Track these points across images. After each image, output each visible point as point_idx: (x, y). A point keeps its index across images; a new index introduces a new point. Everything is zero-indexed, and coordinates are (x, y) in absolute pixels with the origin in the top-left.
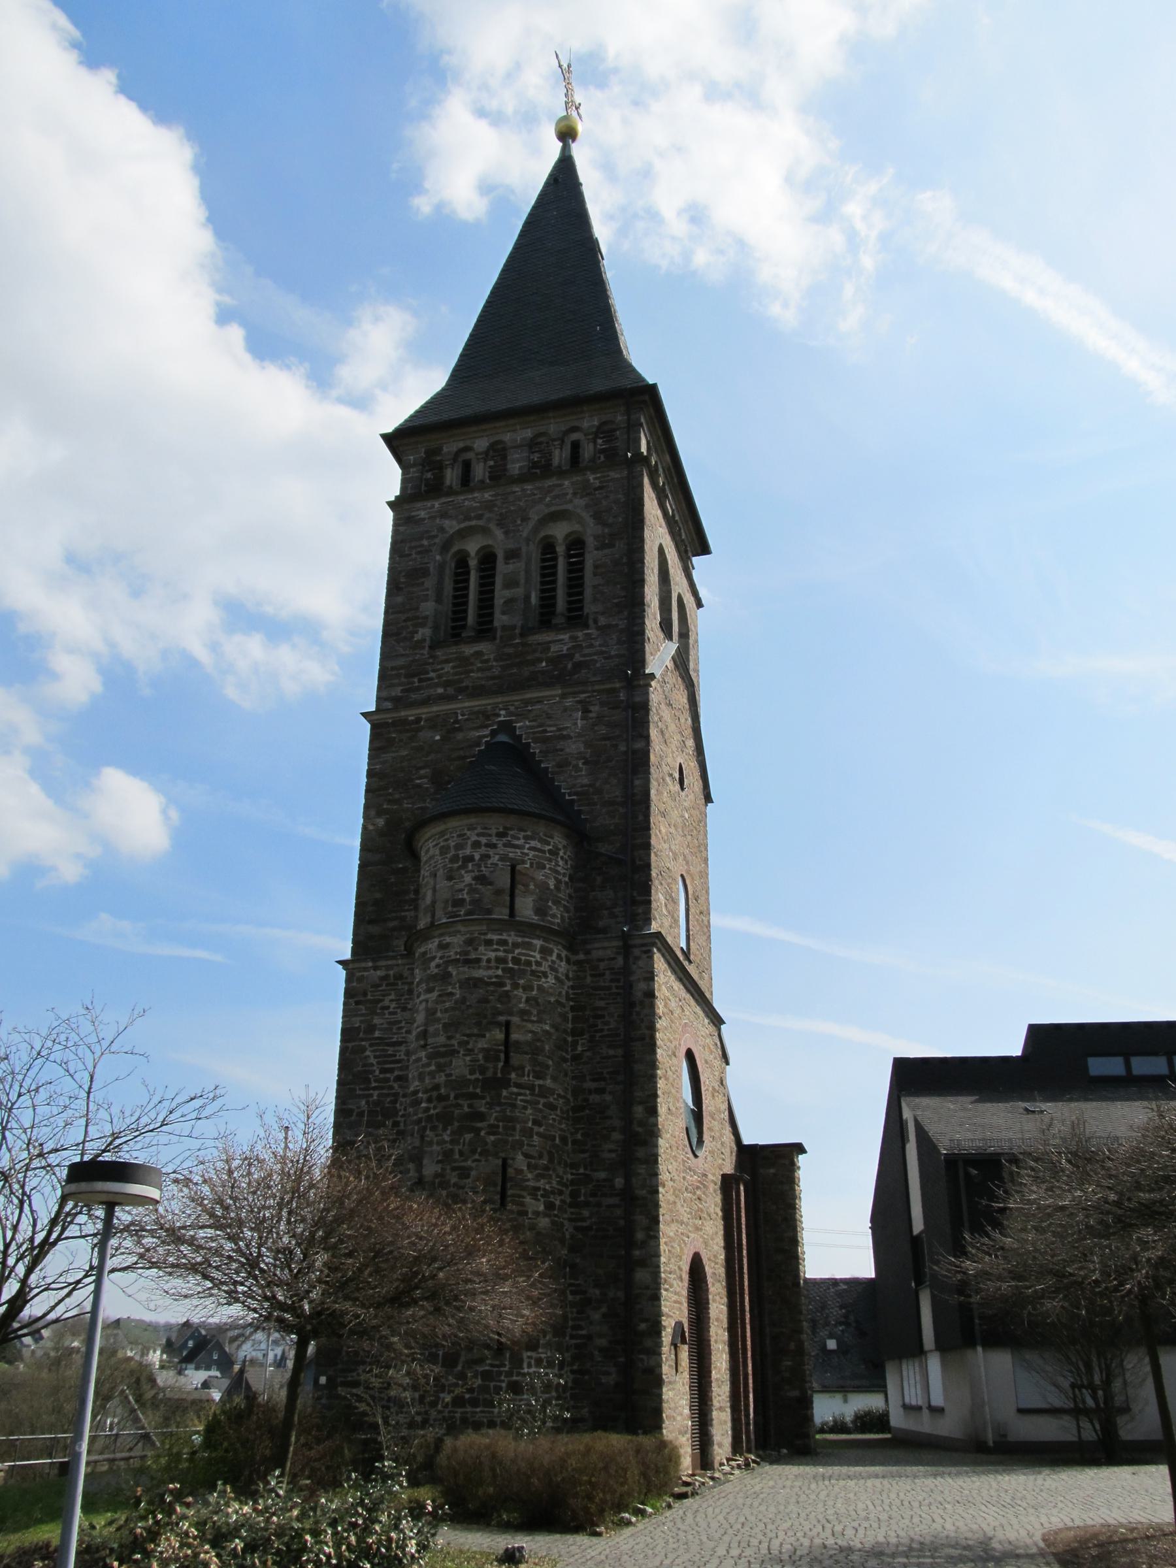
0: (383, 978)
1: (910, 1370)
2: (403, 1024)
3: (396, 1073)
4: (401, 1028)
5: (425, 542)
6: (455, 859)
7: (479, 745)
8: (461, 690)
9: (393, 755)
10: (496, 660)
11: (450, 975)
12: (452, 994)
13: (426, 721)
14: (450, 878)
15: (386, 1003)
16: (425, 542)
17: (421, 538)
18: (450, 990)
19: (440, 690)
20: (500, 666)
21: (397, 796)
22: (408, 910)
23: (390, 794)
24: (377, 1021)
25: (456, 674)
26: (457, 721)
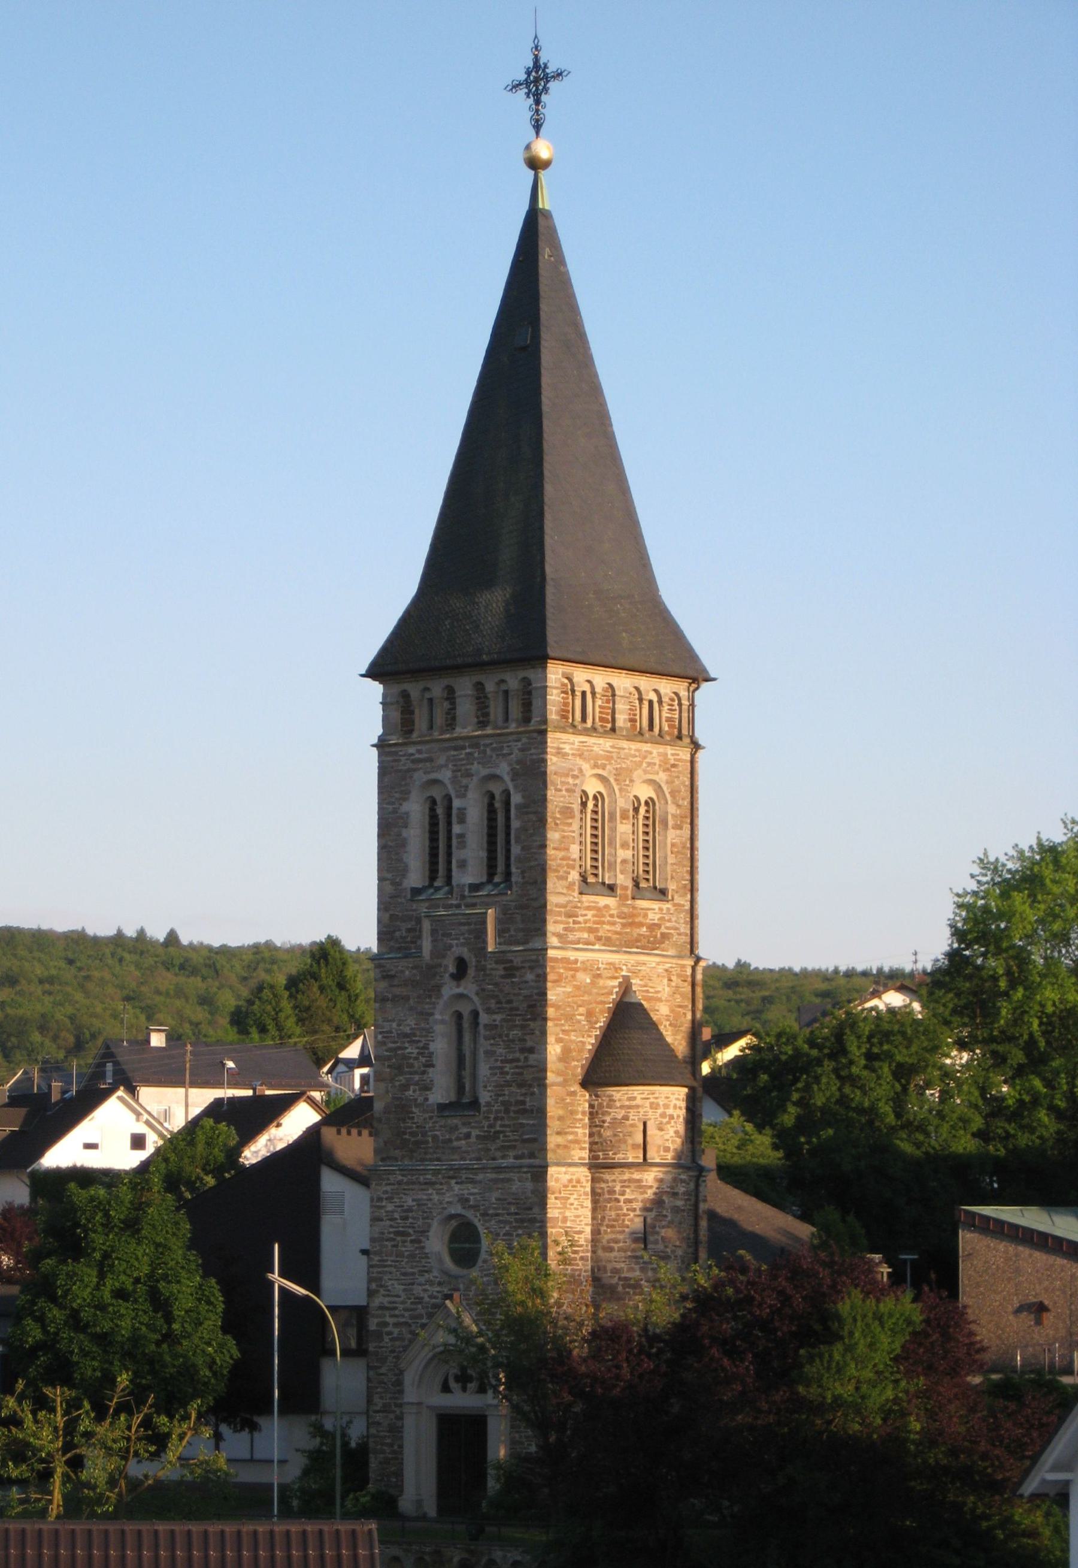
0: (570, 1181)
1: (288, 1480)
2: (582, 1218)
3: (581, 1254)
4: (581, 1221)
5: (571, 780)
6: (663, 1115)
7: (612, 994)
8: (599, 939)
9: (563, 989)
10: (618, 917)
11: (663, 1202)
12: (666, 1216)
13: (581, 962)
14: (661, 1129)
15: (571, 1200)
16: (571, 780)
17: (567, 775)
18: (665, 1213)
19: (586, 935)
20: (621, 923)
21: (567, 1028)
22: (578, 1128)
23: (563, 1025)
24: (568, 1214)
25: (595, 923)
26: (598, 969)
